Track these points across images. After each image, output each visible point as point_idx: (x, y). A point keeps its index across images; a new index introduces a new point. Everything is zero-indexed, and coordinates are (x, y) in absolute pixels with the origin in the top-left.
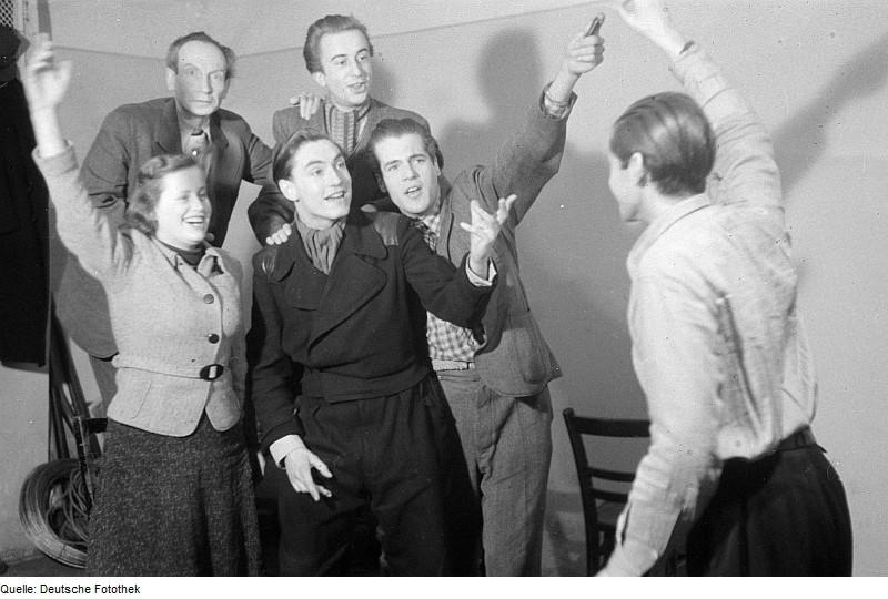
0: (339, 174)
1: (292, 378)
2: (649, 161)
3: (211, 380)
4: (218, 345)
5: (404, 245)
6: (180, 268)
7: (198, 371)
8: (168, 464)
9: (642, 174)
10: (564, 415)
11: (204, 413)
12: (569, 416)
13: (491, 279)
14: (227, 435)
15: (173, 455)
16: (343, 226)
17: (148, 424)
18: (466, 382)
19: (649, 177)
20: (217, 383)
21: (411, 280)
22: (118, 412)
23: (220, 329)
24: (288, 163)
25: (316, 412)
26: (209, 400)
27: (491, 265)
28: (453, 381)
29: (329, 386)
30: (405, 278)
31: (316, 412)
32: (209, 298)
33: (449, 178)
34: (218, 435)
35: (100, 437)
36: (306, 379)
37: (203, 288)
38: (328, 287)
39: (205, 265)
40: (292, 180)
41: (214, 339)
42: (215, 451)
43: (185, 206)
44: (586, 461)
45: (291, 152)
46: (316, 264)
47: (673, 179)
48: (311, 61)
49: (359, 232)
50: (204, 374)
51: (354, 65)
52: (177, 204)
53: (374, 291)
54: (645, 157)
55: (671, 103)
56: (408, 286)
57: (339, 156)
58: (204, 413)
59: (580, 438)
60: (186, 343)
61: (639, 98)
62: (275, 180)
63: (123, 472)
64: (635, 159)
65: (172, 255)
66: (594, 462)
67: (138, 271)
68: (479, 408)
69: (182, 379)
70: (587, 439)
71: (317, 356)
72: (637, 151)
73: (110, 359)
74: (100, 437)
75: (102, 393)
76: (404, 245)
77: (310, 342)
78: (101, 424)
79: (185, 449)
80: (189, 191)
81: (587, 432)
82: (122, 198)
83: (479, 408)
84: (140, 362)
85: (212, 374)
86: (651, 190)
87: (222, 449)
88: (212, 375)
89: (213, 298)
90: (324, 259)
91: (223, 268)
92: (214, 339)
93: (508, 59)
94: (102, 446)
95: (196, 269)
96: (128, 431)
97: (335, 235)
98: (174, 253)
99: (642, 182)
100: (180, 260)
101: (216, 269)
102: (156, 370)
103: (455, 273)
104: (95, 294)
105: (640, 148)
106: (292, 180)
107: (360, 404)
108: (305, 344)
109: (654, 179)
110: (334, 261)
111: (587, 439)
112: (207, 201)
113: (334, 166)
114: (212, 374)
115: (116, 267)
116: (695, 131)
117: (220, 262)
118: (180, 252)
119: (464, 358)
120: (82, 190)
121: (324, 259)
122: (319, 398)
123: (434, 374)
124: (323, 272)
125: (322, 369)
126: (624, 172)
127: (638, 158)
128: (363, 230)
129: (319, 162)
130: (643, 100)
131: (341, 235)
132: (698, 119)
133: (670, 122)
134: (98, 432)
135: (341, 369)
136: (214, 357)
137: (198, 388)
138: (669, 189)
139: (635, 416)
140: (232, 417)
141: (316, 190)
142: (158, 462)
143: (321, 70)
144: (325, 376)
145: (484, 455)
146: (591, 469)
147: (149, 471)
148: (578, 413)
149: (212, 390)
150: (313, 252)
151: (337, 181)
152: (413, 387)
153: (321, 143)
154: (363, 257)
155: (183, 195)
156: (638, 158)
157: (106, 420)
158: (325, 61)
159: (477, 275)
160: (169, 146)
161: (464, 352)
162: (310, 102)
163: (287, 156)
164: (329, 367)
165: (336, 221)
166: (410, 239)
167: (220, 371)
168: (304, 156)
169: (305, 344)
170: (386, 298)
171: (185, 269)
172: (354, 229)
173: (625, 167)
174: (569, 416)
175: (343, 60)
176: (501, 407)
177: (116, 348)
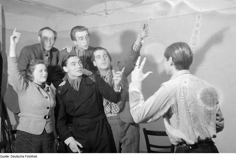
0: (80, 65)
1: (68, 119)
2: (174, 60)
3: (47, 119)
4: (49, 109)
5: (97, 81)
6: (39, 89)
7: (43, 117)
8: (34, 142)
9: (172, 63)
10: (143, 130)
11: (45, 129)
12: (144, 130)
13: (120, 90)
14: (51, 134)
15: (35, 139)
16: (81, 78)
17: (30, 131)
18: (117, 120)
19: (174, 64)
20: (48, 120)
21: (99, 90)
22: (20, 128)
23: (50, 105)
24: (66, 62)
25: (77, 129)
26: (46, 125)
27: (120, 86)
28: (114, 120)
29: (81, 121)
30: (98, 90)
31: (77, 129)
32: (47, 97)
33: (112, 65)
34: (48, 134)
35: (15, 135)
36: (74, 120)
37: (45, 94)
38: (78, 94)
39: (46, 89)
40: (67, 67)
41: (48, 108)
42: (47, 139)
43: (41, 74)
44: (149, 142)
45: (67, 59)
46: (75, 89)
47: (180, 65)
48: (73, 38)
49: (86, 79)
50: (45, 117)
51: (85, 40)
52: (39, 72)
53: (91, 94)
54: (173, 58)
55: (181, 45)
56: (99, 92)
57: (80, 60)
58: (45, 129)
59: (147, 136)
60: (41, 109)
61: (173, 43)
62: (62, 65)
63: (21, 144)
64: (170, 59)
65: (37, 86)
66: (151, 143)
67: (28, 90)
68: (121, 126)
69: (39, 119)
70: (149, 136)
71: (77, 113)
72: (171, 56)
73: (18, 114)
74: (15, 135)
75: (17, 122)
76: (97, 81)
77: (74, 110)
78: (15, 131)
79: (39, 138)
80: (42, 69)
81: (149, 135)
82: (26, 73)
83: (121, 126)
84: (27, 114)
85: (47, 118)
86: (173, 68)
87: (49, 138)
88: (47, 118)
89: (47, 97)
90: (77, 88)
91: (50, 90)
92: (48, 108)
93: (128, 37)
94: (16, 138)
95: (44, 90)
96: (23, 133)
97: (79, 80)
98: (38, 85)
99: (172, 65)
100: (39, 87)
101: (48, 90)
102: (32, 116)
103: (111, 88)
104: (15, 96)
105: (172, 56)
106: (67, 67)
107: (90, 125)
108: (73, 110)
109: (175, 64)
110: (80, 87)
111: (149, 136)
112: (47, 72)
113: (79, 63)
114: (47, 118)
115: (23, 89)
116: (187, 52)
117: (49, 89)
118: (39, 85)
119: (116, 112)
120: (18, 72)
121: (77, 88)
122: (78, 125)
123: (106, 117)
124: (76, 91)
125: (78, 116)
126: (167, 62)
127: (171, 58)
128: (87, 78)
129: (74, 62)
130: (174, 43)
131: (81, 80)
132: (188, 50)
133: (180, 49)
134: (15, 134)
135: (83, 116)
136: (48, 113)
137: (43, 121)
138: (178, 68)
139: (163, 130)
140: (51, 130)
141: (73, 70)
142: (31, 141)
143: (76, 40)
144: (79, 119)
145: (122, 139)
146: (150, 145)
147: (29, 144)
148: (147, 129)
149: (47, 122)
150: (74, 86)
151: (79, 67)
152: (103, 120)
153: (75, 57)
154: (87, 85)
155: (41, 70)
156: (171, 58)
157: (17, 130)
158: (77, 38)
159: (117, 89)
160: (40, 59)
161: (116, 111)
162: (69, 48)
163: (66, 60)
164: (81, 116)
165: (79, 77)
166: (98, 80)
167: (49, 117)
168: (71, 60)
169: (73, 110)
170: (94, 96)
171: (41, 89)
172: (84, 78)
173: (168, 60)
174: (144, 130)
175: (82, 38)
176: (127, 125)
177: (20, 110)
